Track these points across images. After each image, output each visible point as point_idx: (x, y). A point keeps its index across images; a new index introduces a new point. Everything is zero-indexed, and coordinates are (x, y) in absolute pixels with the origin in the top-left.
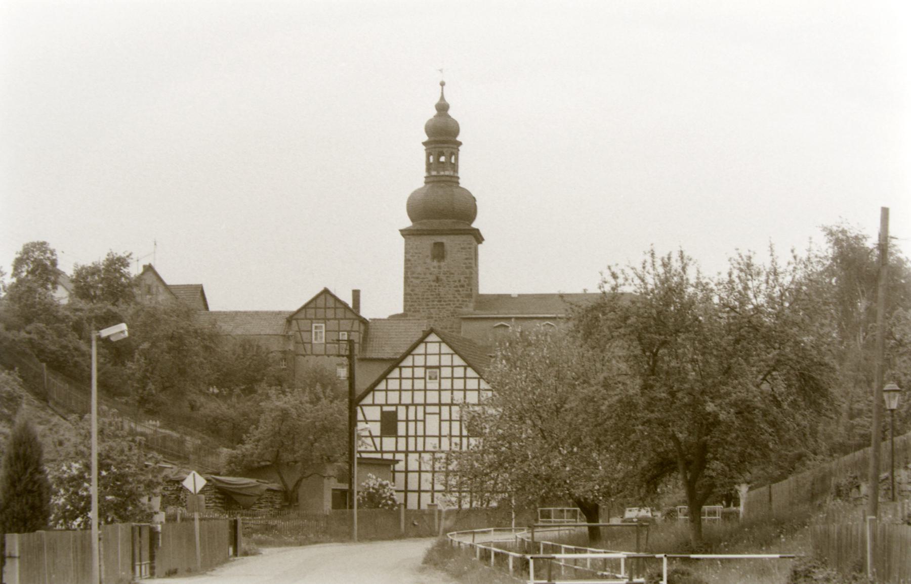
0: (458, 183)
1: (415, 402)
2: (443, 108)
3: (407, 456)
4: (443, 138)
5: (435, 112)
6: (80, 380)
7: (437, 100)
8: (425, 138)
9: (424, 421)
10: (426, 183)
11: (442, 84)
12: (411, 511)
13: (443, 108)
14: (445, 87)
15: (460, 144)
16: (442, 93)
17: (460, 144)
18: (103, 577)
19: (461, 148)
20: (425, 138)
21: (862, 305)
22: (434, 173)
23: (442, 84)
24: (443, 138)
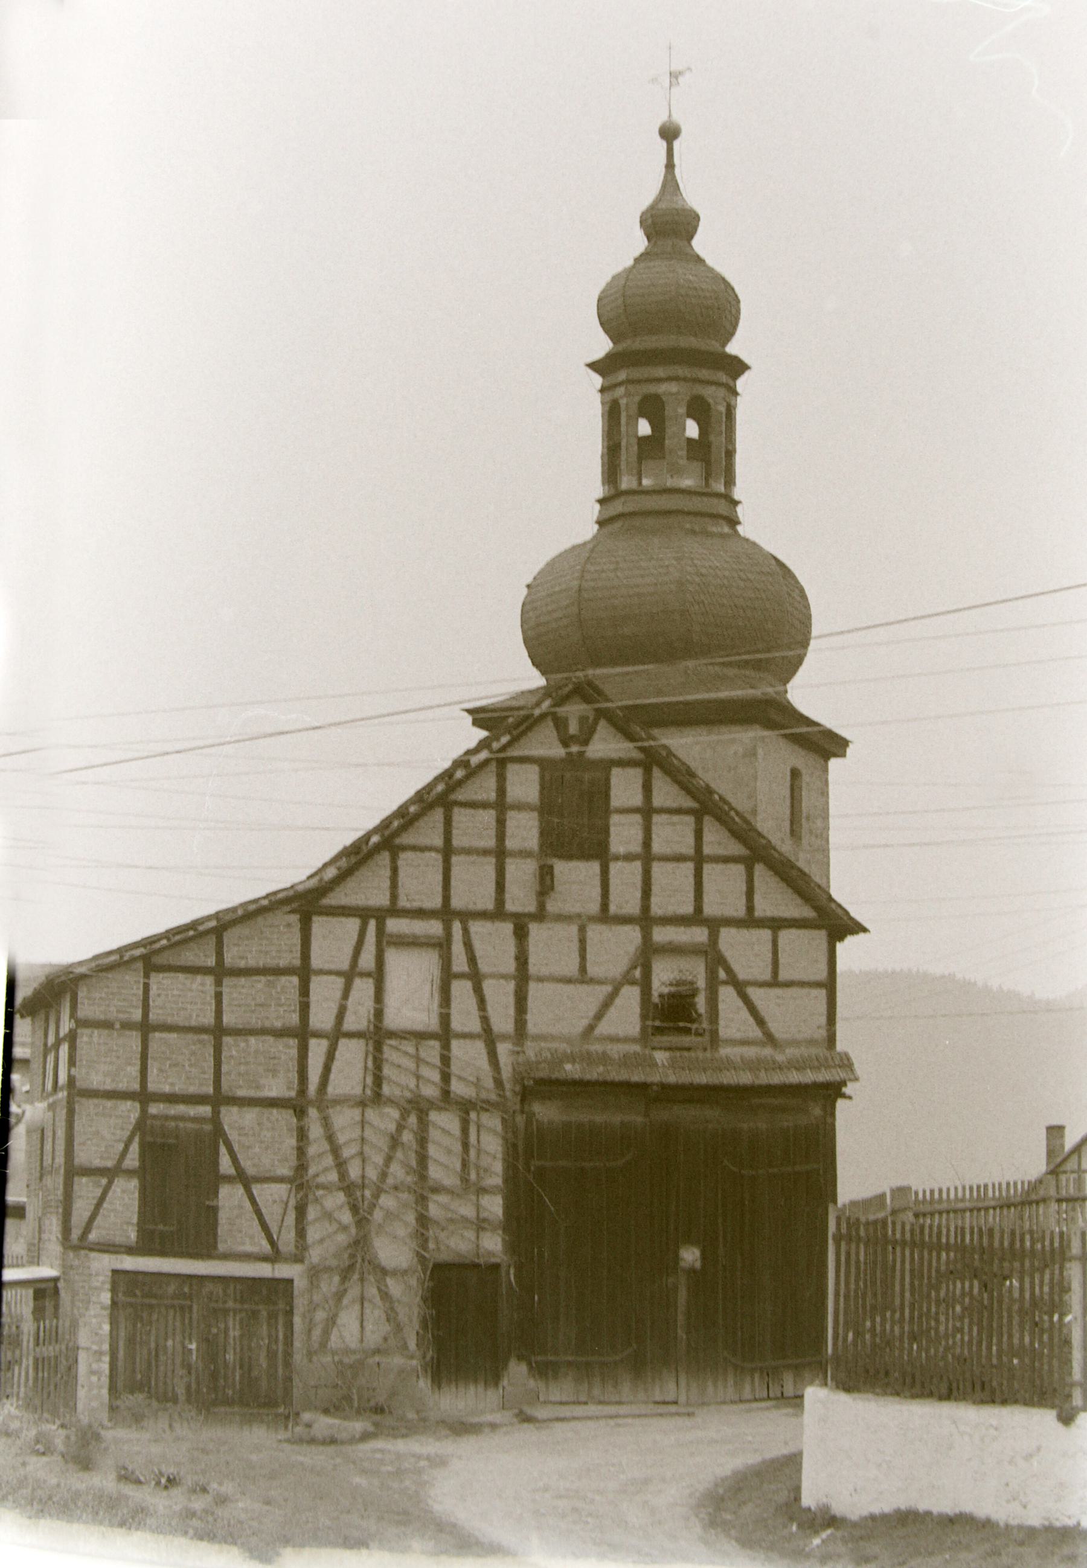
0: (733, 522)
1: (709, 910)
2: (669, 226)
3: (646, 907)
4: (669, 351)
5: (639, 242)
6: (175, 1400)
7: (647, 193)
8: (601, 345)
9: (379, 975)
10: (601, 523)
11: (669, 134)
12: (584, 855)
13: (669, 226)
14: (676, 144)
15: (738, 367)
16: (670, 166)
17: (738, 367)
18: (862, 1258)
19: (741, 384)
20: (601, 345)
21: (932, 1351)
22: (626, 482)
23: (669, 134)
24: (669, 351)
